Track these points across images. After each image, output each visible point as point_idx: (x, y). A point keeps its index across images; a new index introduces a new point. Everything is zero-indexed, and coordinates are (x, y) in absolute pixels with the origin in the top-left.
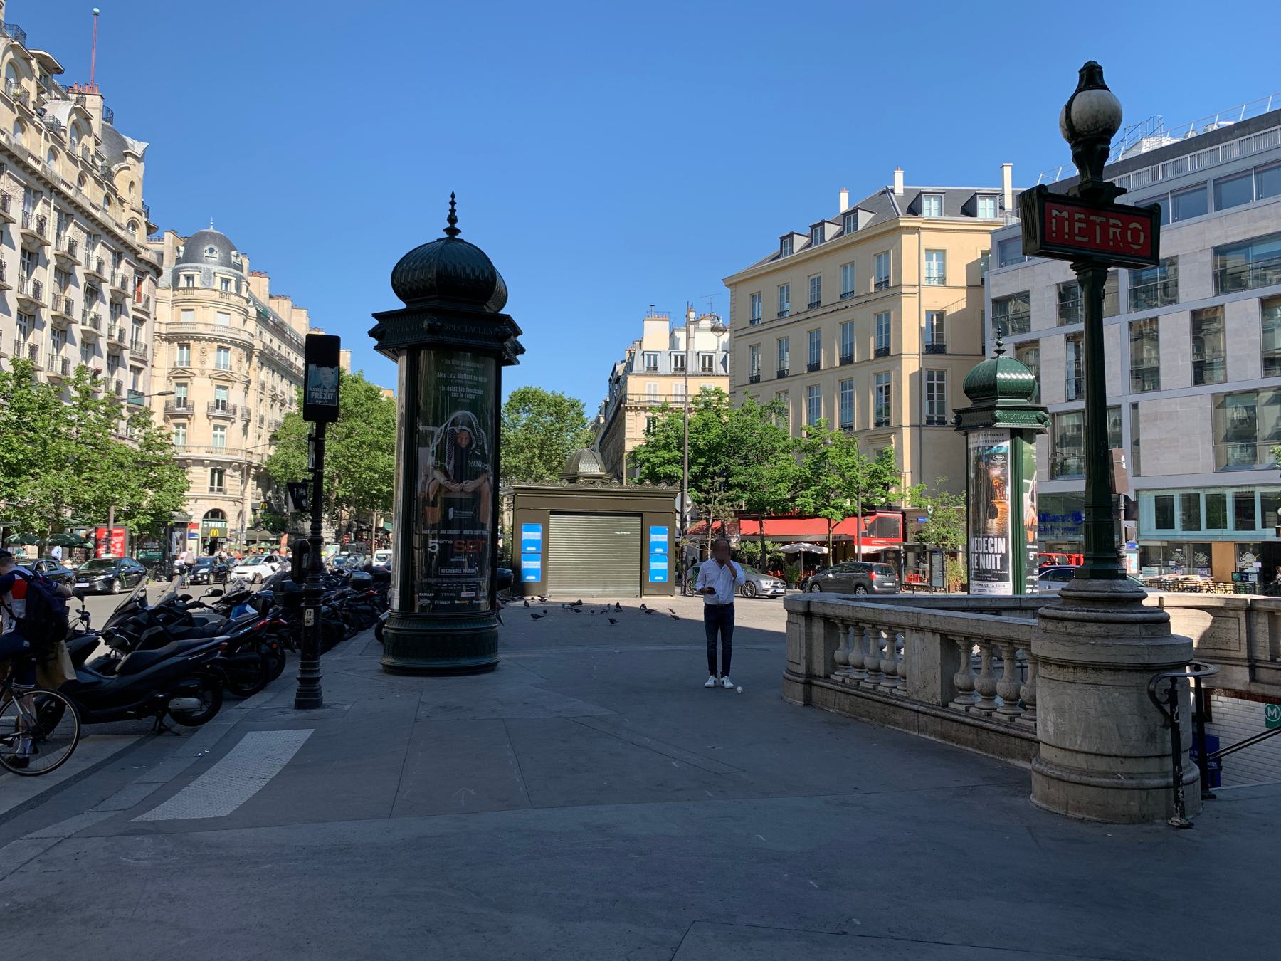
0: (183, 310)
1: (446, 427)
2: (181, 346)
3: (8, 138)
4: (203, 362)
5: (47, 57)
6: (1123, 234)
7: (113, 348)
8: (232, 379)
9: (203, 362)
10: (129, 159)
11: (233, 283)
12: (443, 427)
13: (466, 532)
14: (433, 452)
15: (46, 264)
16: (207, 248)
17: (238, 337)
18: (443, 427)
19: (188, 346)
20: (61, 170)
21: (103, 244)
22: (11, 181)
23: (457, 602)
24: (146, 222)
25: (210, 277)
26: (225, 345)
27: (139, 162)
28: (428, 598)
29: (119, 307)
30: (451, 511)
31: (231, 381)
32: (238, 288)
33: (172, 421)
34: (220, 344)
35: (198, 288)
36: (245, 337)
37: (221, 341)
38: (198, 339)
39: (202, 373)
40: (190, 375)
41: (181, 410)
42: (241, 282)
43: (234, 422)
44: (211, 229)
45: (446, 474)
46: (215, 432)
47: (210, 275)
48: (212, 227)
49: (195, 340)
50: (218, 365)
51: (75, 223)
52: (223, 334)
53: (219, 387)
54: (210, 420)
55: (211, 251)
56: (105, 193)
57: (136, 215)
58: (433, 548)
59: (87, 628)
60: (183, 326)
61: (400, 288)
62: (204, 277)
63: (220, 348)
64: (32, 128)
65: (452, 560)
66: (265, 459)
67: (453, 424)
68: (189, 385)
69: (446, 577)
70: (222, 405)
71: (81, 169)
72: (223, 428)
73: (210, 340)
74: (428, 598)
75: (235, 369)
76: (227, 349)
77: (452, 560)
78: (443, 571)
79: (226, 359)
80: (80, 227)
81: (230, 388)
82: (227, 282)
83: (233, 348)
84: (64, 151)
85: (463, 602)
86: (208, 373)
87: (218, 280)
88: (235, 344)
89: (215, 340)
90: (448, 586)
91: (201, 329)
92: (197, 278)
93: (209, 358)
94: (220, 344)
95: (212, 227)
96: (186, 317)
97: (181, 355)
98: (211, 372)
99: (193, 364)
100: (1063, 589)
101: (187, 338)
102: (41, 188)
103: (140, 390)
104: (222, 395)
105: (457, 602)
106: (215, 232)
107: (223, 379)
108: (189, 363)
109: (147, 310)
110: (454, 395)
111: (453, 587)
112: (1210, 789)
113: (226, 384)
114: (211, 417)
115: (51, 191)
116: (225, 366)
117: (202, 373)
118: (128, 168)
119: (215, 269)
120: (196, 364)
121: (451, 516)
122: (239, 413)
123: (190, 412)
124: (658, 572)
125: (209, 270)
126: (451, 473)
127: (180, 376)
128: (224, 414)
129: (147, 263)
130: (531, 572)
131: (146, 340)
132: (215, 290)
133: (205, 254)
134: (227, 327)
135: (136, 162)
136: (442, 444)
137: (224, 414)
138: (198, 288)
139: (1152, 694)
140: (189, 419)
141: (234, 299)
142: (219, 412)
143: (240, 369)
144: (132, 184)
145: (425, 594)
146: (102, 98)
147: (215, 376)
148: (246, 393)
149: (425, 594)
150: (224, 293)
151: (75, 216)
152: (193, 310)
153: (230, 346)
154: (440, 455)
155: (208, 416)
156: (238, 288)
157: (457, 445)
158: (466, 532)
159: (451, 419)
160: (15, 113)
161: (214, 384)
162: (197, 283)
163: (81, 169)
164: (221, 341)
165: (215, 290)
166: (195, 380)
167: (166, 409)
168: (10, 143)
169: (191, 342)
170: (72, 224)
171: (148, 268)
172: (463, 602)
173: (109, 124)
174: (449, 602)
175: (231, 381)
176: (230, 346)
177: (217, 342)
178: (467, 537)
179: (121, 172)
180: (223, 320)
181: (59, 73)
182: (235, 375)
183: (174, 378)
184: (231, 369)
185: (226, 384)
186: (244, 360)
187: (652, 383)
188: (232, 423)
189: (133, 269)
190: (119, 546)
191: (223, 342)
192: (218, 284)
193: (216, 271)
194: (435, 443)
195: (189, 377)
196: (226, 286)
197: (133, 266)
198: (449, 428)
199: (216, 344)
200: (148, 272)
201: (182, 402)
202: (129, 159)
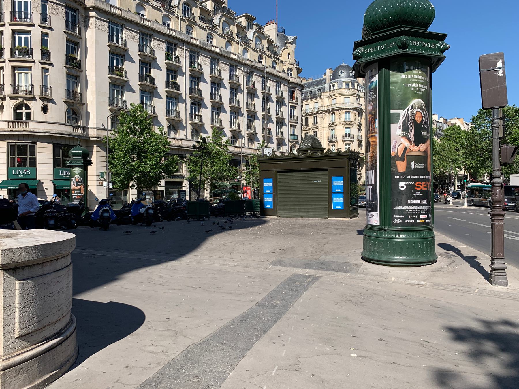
0: (332, 99)
1: (408, 110)
2: (332, 114)
3: (220, 49)
5: (248, 15)
7: (278, 119)
8: (352, 124)
9: (340, 119)
10: (287, 45)
11: (350, 84)
12: (406, 110)
13: (422, 177)
14: (400, 126)
15: (242, 92)
16: (339, 72)
17: (353, 106)
18: (406, 110)
19: (334, 113)
20: (251, 57)
21: (270, 80)
22: (223, 64)
23: (418, 221)
24: (296, 67)
25: (341, 84)
26: (348, 110)
27: (292, 44)
28: (400, 218)
30: (413, 163)
31: (351, 125)
32: (353, 86)
33: (330, 144)
34: (346, 110)
35: (337, 89)
36: (356, 106)
37: (346, 109)
38: (337, 110)
39: (340, 124)
40: (335, 125)
41: (333, 139)
42: (354, 83)
43: (354, 142)
44: (343, 64)
45: (410, 141)
46: (346, 147)
47: (341, 83)
48: (343, 63)
49: (336, 111)
50: (345, 119)
51: (255, 74)
52: (346, 106)
53: (346, 128)
54: (343, 142)
55: (341, 73)
56: (273, 60)
57: (291, 66)
58: (402, 187)
60: (332, 106)
62: (339, 84)
63: (346, 112)
64: (235, 43)
65: (414, 195)
67: (412, 108)
68: (335, 129)
69: (411, 205)
70: (348, 135)
71: (259, 53)
72: (349, 145)
73: (342, 109)
74: (400, 218)
76: (349, 112)
77: (414, 195)
78: (409, 202)
79: (349, 116)
80: (258, 76)
81: (351, 128)
82: (348, 84)
83: (351, 111)
84: (251, 48)
85: (421, 221)
86: (342, 123)
87: (344, 84)
88: (352, 109)
89: (344, 109)
90: (412, 211)
91: (338, 106)
92: (336, 85)
93: (342, 117)
94: (346, 110)
95: (343, 63)
96: (334, 102)
97: (332, 118)
98: (343, 122)
99: (336, 121)
101: (334, 110)
102: (238, 64)
103: (296, 134)
104: (348, 131)
105: (418, 221)
106: (345, 64)
107: (348, 125)
108: (335, 120)
109: (297, 103)
110: (413, 89)
111: (416, 211)
113: (349, 126)
114: (343, 141)
115: (242, 64)
116: (349, 119)
117: (340, 124)
118: (287, 48)
119: (343, 80)
120: (337, 120)
121: (413, 167)
122: (355, 138)
123: (336, 140)
124: (337, 204)
125: (340, 81)
126: (412, 139)
127: (332, 126)
128: (349, 139)
129: (295, 83)
130: (268, 203)
131: (297, 114)
132: (343, 89)
133: (339, 75)
135: (290, 45)
136: (405, 123)
137: (349, 139)
138: (337, 89)
140: (336, 143)
141: (351, 91)
142: (347, 139)
143: (355, 119)
144: (289, 54)
145: (398, 216)
146: (276, 24)
147: (344, 124)
148: (359, 129)
149: (398, 216)
150: (347, 89)
151: (255, 71)
152: (335, 98)
153: (350, 110)
154: (405, 128)
155: (342, 140)
156: (353, 86)
157: (415, 121)
158: (422, 177)
159: (411, 105)
160: (226, 39)
161: (344, 127)
162: (336, 87)
163: (259, 53)
164: (346, 109)
165: (343, 89)
166: (337, 127)
167: (328, 140)
168: (221, 51)
169: (335, 112)
170: (254, 75)
171: (295, 86)
172: (421, 221)
173: (283, 34)
174: (413, 221)
175: (351, 125)
176: (350, 110)
177: (345, 110)
178: (424, 180)
179: (284, 51)
180: (347, 100)
181: (255, 20)
182: (353, 122)
183: (330, 127)
185: (349, 126)
186: (357, 116)
188: (353, 142)
189: (287, 87)
190: (249, 193)
191: (347, 110)
192: (344, 86)
193: (343, 80)
194: (401, 121)
195: (335, 126)
196: (348, 86)
197: (287, 86)
198: (410, 111)
199: (344, 111)
200: (296, 87)
201: (333, 136)
202: (287, 45)
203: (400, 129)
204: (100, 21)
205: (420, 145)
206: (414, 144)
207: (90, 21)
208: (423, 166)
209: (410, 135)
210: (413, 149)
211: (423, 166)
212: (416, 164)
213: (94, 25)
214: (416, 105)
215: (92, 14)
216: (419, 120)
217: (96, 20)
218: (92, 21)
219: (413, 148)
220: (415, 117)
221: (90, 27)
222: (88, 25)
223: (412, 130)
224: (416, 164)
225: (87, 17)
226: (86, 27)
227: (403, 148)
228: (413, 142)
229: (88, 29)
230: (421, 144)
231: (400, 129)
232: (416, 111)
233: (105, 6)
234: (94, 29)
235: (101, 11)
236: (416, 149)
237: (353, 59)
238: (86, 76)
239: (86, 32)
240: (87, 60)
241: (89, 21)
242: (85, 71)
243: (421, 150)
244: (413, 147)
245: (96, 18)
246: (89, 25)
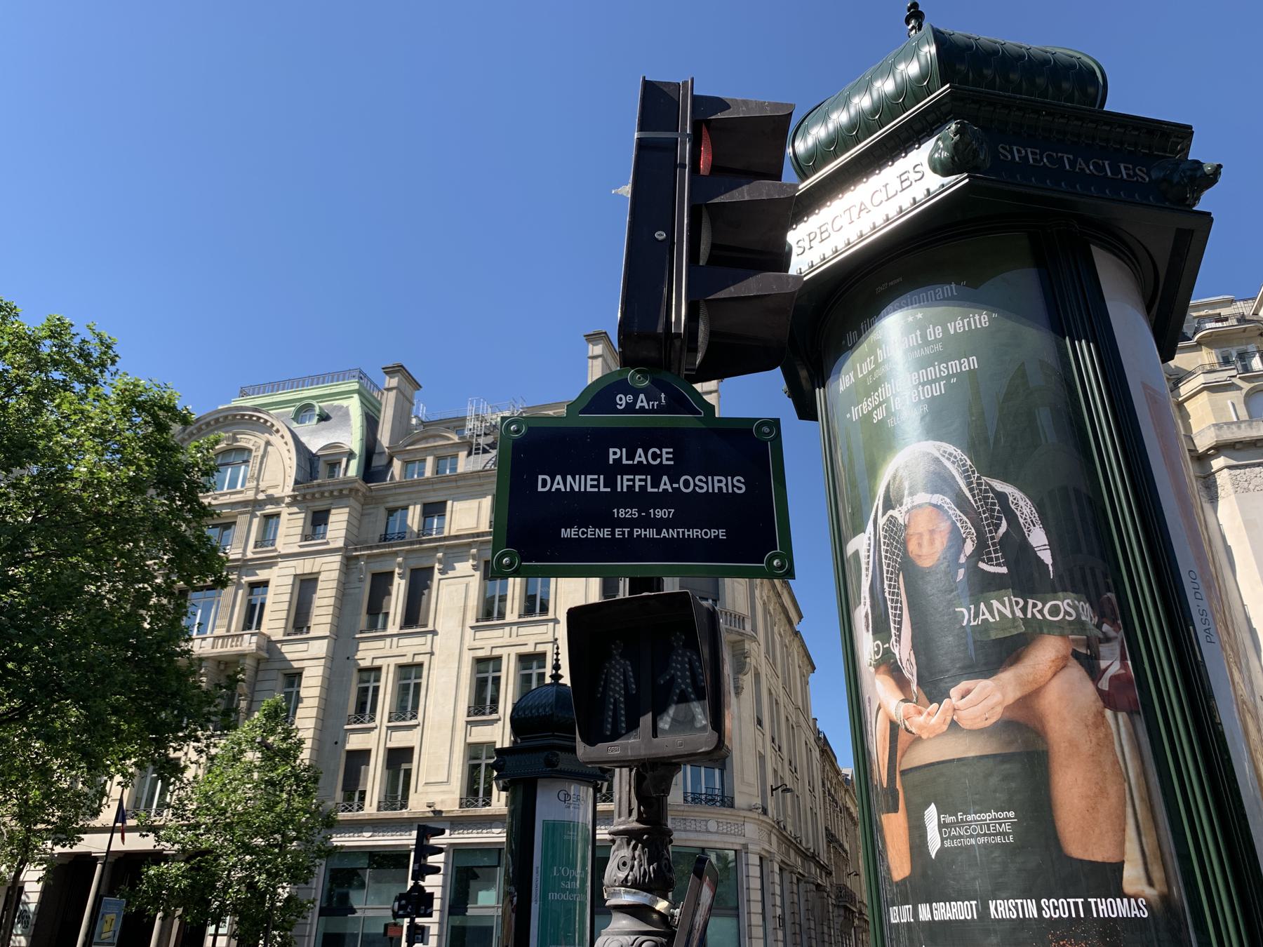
159: (881, 492)
198: (882, 521)
203: (868, 630)
204: (1242, 471)
205: (953, 692)
206: (923, 698)
207: (1219, 481)
208: (1006, 828)
209: (896, 652)
210: (921, 727)
211: (1006, 828)
212: (949, 819)
213: (1229, 487)
214: (901, 483)
215: (1217, 463)
216: (925, 550)
217: (1232, 472)
218: (1223, 479)
219: (921, 719)
220: (905, 544)
221: (1222, 495)
222: (1217, 492)
223: (901, 616)
224: (949, 819)
225: (1209, 475)
226: (1214, 499)
227: (885, 729)
228: (914, 687)
229: (1221, 503)
230: (964, 685)
231: (868, 630)
232: (904, 508)
233: (1249, 429)
234: (1233, 496)
235: (1238, 446)
236: (934, 720)
237: (779, 419)
238: (1248, 620)
239: (1216, 512)
240: (1238, 579)
241: (1216, 482)
242: (1241, 608)
243: (965, 724)
244: (920, 713)
245: (1230, 467)
246: (1219, 491)
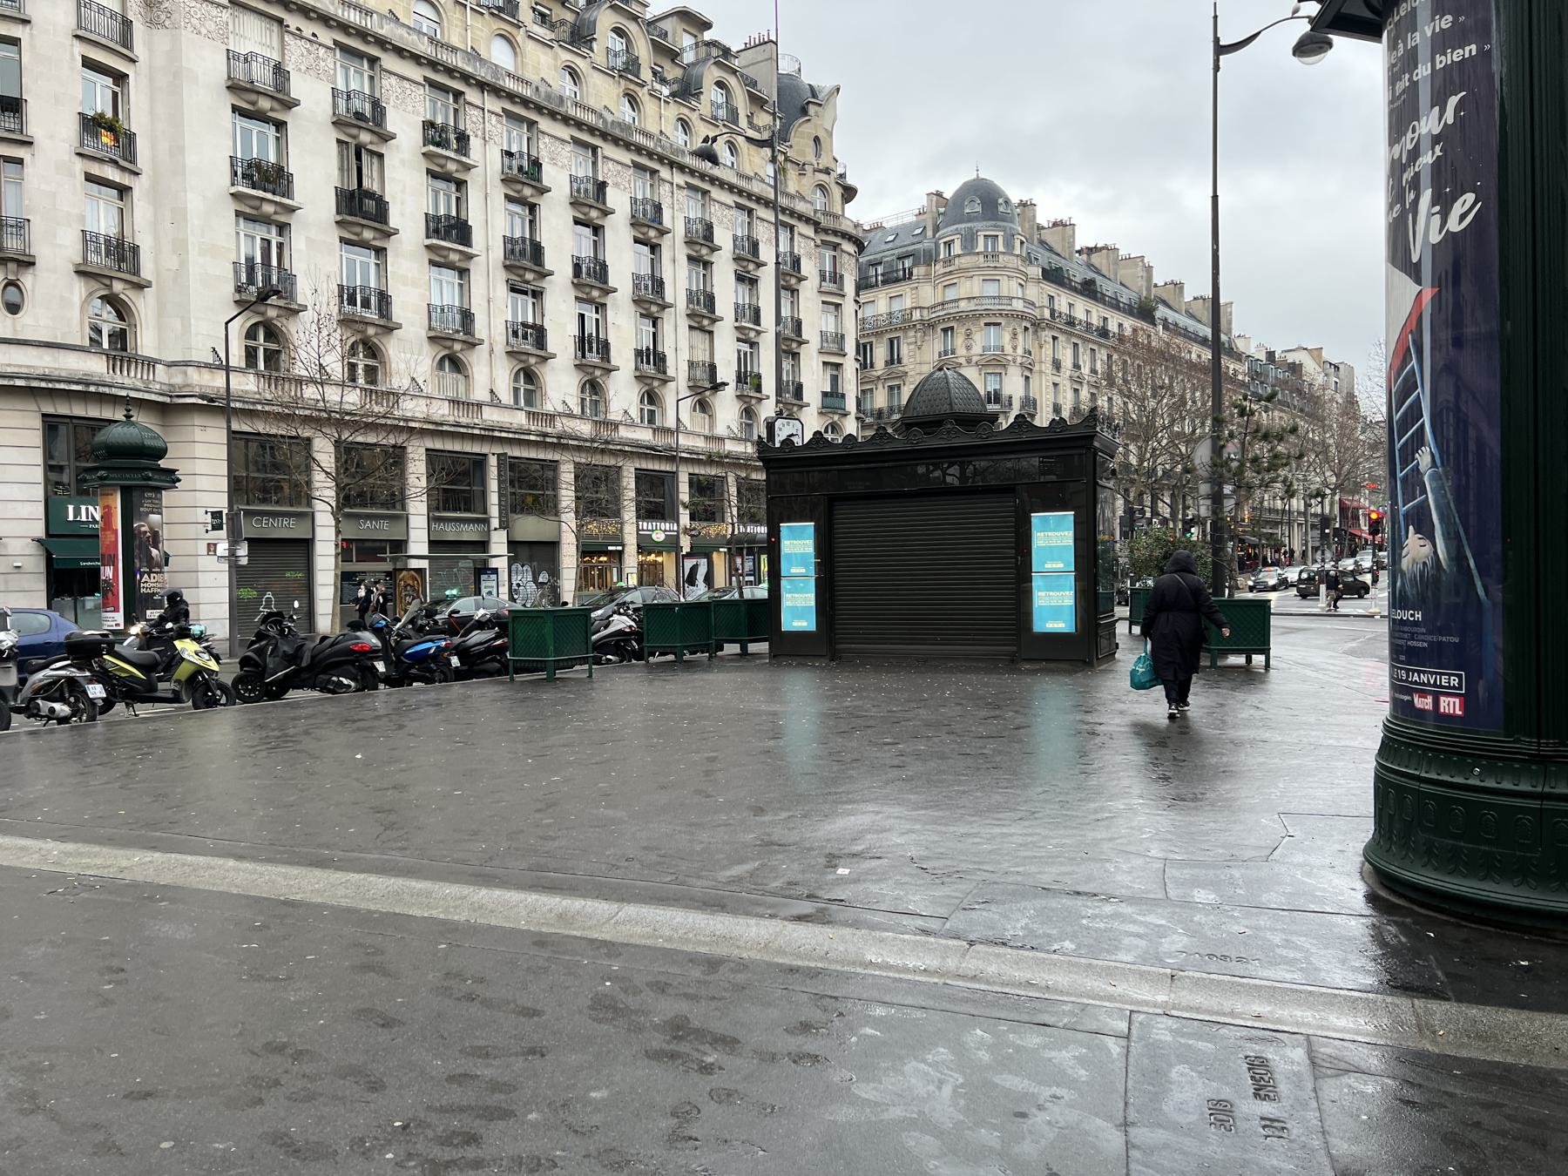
4: (968, 348)
6: (1286, 884)
9: (968, 348)
29: (796, 293)
39: (969, 361)
52: (989, 307)
59: (229, 422)
61: (1330, 45)
66: (1209, 469)
75: (1008, 349)
86: (975, 359)
98: (979, 358)
100: (301, 742)
112: (105, 657)
117: (969, 361)
134: (994, 298)
139: (656, 1055)
143: (1015, 348)
168: (605, 121)
184: (1003, 351)
187: (359, 259)
